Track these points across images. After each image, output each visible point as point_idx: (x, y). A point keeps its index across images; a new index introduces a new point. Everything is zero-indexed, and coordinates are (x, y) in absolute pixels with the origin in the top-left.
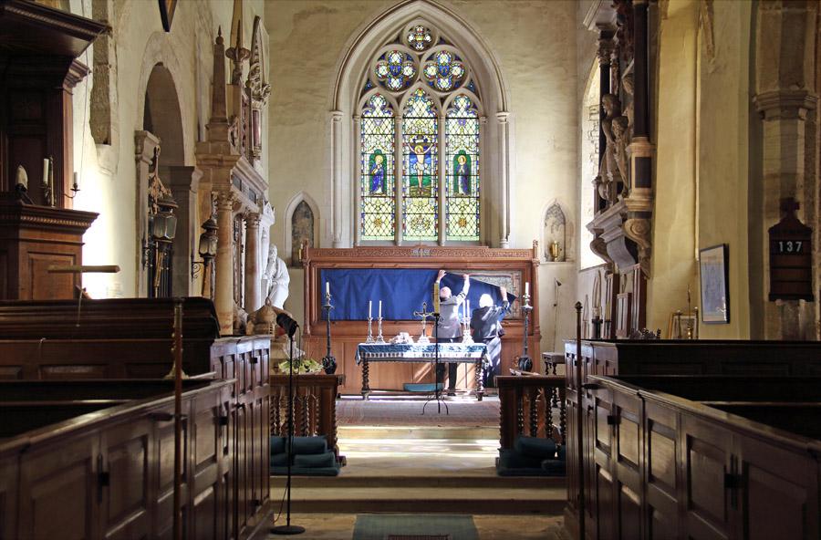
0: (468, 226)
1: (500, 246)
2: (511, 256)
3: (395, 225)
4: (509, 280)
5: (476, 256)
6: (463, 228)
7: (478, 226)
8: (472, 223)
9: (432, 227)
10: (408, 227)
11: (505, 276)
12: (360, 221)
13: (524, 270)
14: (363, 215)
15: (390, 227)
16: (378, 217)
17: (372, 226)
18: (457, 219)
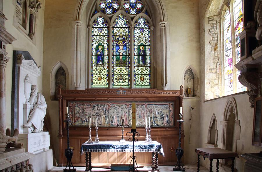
0: (145, 81)
1: (163, 89)
2: (169, 94)
4: (167, 106)
5: (138, 94)
6: (142, 82)
7: (150, 80)
9: (127, 81)
10: (115, 81)
11: (166, 105)
15: (106, 81)
16: (100, 76)
17: (139, 81)
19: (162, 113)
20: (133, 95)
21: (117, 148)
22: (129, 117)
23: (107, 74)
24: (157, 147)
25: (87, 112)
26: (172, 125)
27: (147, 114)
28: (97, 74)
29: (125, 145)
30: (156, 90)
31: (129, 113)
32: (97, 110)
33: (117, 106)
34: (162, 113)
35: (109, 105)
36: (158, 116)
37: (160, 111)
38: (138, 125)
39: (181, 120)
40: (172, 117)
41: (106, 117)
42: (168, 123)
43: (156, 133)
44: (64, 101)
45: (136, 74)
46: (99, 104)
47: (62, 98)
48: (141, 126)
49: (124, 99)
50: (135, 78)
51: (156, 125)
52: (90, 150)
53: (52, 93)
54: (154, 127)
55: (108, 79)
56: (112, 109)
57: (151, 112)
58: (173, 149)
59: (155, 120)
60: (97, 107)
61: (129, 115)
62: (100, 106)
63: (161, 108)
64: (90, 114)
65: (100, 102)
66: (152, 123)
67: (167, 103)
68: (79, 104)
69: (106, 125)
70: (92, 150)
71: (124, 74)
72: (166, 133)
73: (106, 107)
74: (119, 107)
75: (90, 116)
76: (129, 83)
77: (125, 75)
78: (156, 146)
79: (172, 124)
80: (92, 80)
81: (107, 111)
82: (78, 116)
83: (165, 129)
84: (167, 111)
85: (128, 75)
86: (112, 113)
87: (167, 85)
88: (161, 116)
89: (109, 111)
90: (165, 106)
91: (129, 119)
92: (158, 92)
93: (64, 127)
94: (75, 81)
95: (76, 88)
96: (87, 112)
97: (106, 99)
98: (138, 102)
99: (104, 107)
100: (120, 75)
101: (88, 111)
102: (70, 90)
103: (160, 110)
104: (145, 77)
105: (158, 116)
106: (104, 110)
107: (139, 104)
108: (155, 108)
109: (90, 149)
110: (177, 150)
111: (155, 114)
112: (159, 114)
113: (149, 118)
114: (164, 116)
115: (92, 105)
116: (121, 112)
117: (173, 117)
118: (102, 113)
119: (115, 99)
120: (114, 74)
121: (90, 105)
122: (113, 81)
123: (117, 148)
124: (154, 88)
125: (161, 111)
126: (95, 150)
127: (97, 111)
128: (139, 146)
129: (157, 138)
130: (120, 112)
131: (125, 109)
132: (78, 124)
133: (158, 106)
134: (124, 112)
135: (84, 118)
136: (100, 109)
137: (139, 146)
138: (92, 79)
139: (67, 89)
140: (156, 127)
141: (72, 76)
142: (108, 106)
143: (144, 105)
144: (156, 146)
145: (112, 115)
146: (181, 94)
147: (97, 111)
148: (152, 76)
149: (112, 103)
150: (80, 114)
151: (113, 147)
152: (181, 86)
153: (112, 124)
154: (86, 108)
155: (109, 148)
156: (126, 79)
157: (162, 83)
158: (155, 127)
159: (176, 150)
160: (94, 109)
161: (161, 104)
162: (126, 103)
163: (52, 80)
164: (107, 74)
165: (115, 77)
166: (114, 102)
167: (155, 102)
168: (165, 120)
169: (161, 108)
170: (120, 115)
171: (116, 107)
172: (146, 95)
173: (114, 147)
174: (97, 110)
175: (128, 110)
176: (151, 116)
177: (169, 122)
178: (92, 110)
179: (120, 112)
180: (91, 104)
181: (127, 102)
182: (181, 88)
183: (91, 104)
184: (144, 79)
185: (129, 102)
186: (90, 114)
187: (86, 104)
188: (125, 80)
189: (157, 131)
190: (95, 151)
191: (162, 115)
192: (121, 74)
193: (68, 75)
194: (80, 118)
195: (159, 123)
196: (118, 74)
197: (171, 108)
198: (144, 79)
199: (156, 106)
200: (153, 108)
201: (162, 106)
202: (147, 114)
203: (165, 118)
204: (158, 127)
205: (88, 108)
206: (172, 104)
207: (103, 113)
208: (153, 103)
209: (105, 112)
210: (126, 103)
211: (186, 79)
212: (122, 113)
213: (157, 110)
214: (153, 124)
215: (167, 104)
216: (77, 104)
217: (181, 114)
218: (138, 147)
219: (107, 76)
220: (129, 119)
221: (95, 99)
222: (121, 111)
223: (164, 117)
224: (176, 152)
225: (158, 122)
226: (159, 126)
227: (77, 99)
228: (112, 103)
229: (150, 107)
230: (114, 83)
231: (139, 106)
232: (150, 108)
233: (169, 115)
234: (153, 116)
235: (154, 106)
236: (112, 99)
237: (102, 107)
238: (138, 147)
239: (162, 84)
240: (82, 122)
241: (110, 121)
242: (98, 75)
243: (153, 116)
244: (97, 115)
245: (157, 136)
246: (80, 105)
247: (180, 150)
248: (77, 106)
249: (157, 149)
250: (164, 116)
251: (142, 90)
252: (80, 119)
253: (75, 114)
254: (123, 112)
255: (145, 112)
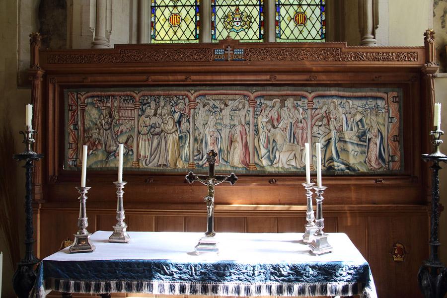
0: (309, 25)
1: (363, 43)
2: (388, 59)
3: (199, 24)
4: (379, 102)
5: (284, 59)
6: (301, 28)
7: (324, 23)
8: (189, 20)
9: (255, 26)
10: (220, 26)
11: (376, 98)
12: (146, 20)
13: (62, 87)
14: (153, 9)
15: (192, 26)
16: (175, 11)
17: (292, 24)
18: (292, 12)
19: (363, 126)
20: (267, 64)
21: (181, 278)
22: (256, 140)
23: (196, 5)
24: (349, 276)
25: (121, 122)
26: (396, 166)
27: (315, 129)
28: (167, 6)
29: (217, 266)
30: (345, 47)
31: (256, 125)
32: (155, 115)
33: (217, 103)
34: (363, 126)
35: (192, 98)
36: (349, 135)
37: (358, 117)
38: (286, 167)
39: (439, 154)
40: (396, 139)
41: (181, 138)
42: (384, 160)
43: (344, 195)
44: (51, 87)
45: (283, 5)
46: (159, 96)
47: (45, 76)
48: (293, 170)
49: (239, 78)
50: (280, 15)
51: (343, 166)
52: (72, 282)
53: (22, 64)
54: (336, 173)
55: (198, 19)
56: (202, 113)
57: (328, 122)
58: (402, 252)
59: (339, 150)
60: (153, 105)
61: (257, 131)
62: (162, 103)
63: (360, 109)
64: (132, 128)
65: (163, 90)
66: (331, 159)
67: (379, 91)
68: (98, 96)
69: (180, 165)
70: (83, 283)
71: (246, 5)
72: (376, 196)
73: (181, 106)
74: (223, 106)
75: (131, 136)
76: (262, 33)
77: (251, 8)
78: (344, 274)
79: (398, 164)
80: (153, 25)
81: (184, 120)
82: (95, 136)
83: (373, 182)
84: (381, 121)
85: (258, 7)
86: (201, 127)
87: (377, 31)
88: (362, 136)
89: (191, 120)
90: (374, 103)
91: (256, 144)
92: (348, 53)
93: (51, 173)
94: (92, 24)
95: (94, 44)
96: (121, 122)
97: (183, 77)
98: (286, 88)
99: (176, 104)
100: (233, 9)
101: (125, 118)
102: (79, 51)
103: (355, 115)
104: (309, 13)
105: (349, 135)
106: (177, 116)
107: (288, 96)
108: (341, 110)
109: (75, 278)
110: (425, 269)
111: (339, 131)
112: (355, 128)
113: (319, 146)
114: (369, 136)
115: (137, 99)
116: (228, 122)
117: (399, 142)
118: (170, 126)
119: (209, 78)
120: (215, 6)
121: (133, 98)
122: (213, 26)
123: (184, 277)
124: (337, 39)
125: (361, 120)
126: (93, 283)
127: (154, 120)
128: (274, 268)
129: (348, 215)
130: (227, 121)
131: (243, 112)
132: (96, 163)
133: (351, 102)
134: (240, 123)
135: (112, 143)
136: (161, 113)
137: (274, 268)
138: (152, 23)
139: (68, 47)
140: (343, 175)
141: (82, 9)
142: (187, 101)
143: (305, 97)
144: (344, 274)
145: (202, 131)
146: (427, 61)
147: (154, 120)
148: (330, 8)
149: (201, 92)
150: (100, 130)
151: (165, 274)
152: (425, 34)
153: (201, 163)
154: (120, 108)
155: (151, 277)
156: (253, 20)
157: (360, 27)
158: (340, 172)
159: (422, 272)
160: (143, 111)
161: (360, 94)
162: (245, 93)
163: (21, 23)
164: (196, 5)
165: (220, 13)
166: (207, 88)
167: (341, 89)
168: (374, 151)
169: (360, 109)
170: (225, 133)
171: (214, 107)
172: (308, 64)
173: (171, 275)
174: (155, 115)
175: (251, 114)
176: (327, 138)
177: (385, 156)
178: (139, 115)
179: (227, 121)
180: (135, 95)
181: (250, 88)
182: (426, 39)
183: (135, 95)
184: (305, 19)
185: (256, 88)
186: (132, 128)
187: (120, 96)
188: (251, 22)
189: (347, 188)
190: (93, 287)
191: (364, 134)
192: (236, 5)
193: (72, 5)
194: (101, 144)
195: (352, 161)
196: (229, 6)
197: (394, 108)
198: (305, 19)
199: (344, 101)
200: (332, 108)
201: (364, 102)
202: (315, 129)
203: (371, 144)
204: (352, 173)
205: (126, 109)
206: (395, 94)
207: (171, 127)
208: (333, 93)
209: (179, 122)
210: (245, 93)
211: (440, 13)
212: (234, 126)
213: (349, 116)
214: (336, 164)
215: (379, 94)
216: (93, 97)
217: (439, 130)
218: (272, 274)
219: (197, 12)
220: (256, 144)
221: (147, 80)
222: (228, 117)
223: (369, 140)
224: (420, 279)
225: (351, 157)
226: (354, 170)
227: (90, 79)
228: (201, 92)
229: (323, 106)
230: (218, 33)
231: (289, 102)
232: (324, 109)
233: (385, 134)
234: (333, 134)
235: (337, 101)
236: (202, 77)
237: (169, 107)
238: (272, 274)
239: (363, 31)
240: (108, 158)
241: (196, 153)
242: (171, 9)
243: (333, 134)
244: (156, 133)
245: (346, 207)
246: (101, 99)
247: (435, 272)
248: (92, 104)
249: (351, 285)
250: (369, 136)
251: (296, 47)
252: (100, 147)
253: (84, 131)
254: (236, 122)
255: (309, 124)
